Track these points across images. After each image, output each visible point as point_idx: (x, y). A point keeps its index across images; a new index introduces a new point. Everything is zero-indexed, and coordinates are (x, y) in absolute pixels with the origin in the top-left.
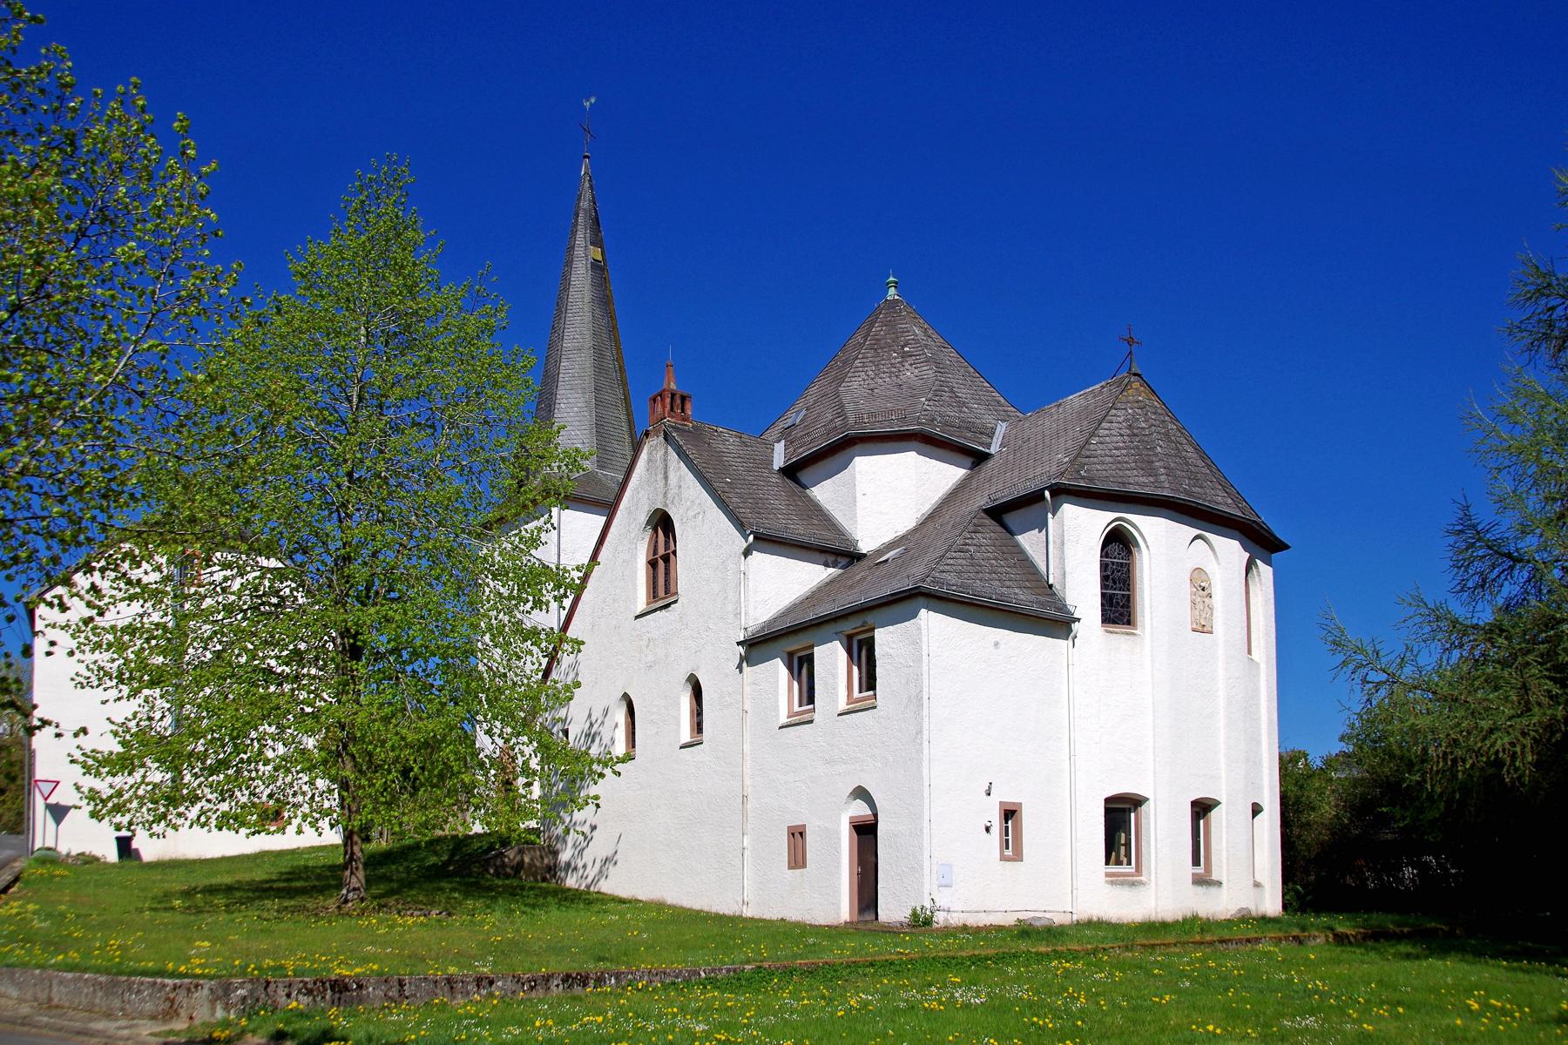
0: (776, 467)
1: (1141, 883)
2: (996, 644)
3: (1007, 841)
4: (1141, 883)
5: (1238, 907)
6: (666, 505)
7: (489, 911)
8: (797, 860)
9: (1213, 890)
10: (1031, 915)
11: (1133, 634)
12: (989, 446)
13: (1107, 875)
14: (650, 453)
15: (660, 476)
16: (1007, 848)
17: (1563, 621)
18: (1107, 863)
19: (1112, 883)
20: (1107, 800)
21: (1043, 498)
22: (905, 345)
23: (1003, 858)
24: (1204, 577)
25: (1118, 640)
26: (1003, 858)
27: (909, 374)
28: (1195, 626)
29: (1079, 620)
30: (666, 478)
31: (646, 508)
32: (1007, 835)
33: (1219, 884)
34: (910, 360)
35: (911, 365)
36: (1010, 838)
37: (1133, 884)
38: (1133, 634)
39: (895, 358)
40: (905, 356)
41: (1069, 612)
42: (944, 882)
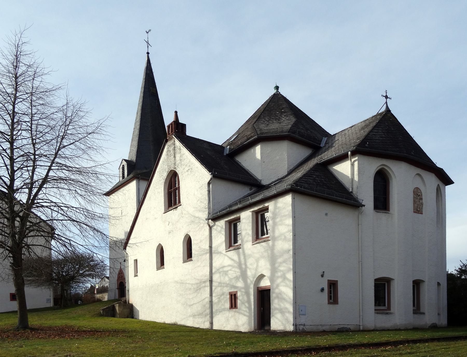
0: (225, 154)
1: (391, 313)
2: (326, 214)
3: (331, 296)
4: (391, 313)
5: (432, 323)
6: (175, 168)
7: (169, 339)
8: (161, 262)
9: (422, 316)
10: (342, 326)
11: (388, 213)
12: (320, 144)
13: (375, 310)
14: (167, 148)
15: (172, 157)
16: (331, 299)
17: (331, 356)
18: (375, 305)
19: (378, 313)
20: (376, 280)
21: (330, 294)
22: (282, 109)
23: (329, 303)
24: (419, 191)
25: (382, 216)
26: (329, 303)
27: (283, 119)
28: (415, 211)
29: (364, 206)
30: (175, 157)
31: (167, 170)
32: (331, 293)
33: (424, 313)
34: (285, 114)
35: (284, 116)
36: (332, 290)
37: (387, 314)
38: (388, 213)
39: (278, 114)
40: (282, 113)
41: (359, 202)
42: (302, 313)
